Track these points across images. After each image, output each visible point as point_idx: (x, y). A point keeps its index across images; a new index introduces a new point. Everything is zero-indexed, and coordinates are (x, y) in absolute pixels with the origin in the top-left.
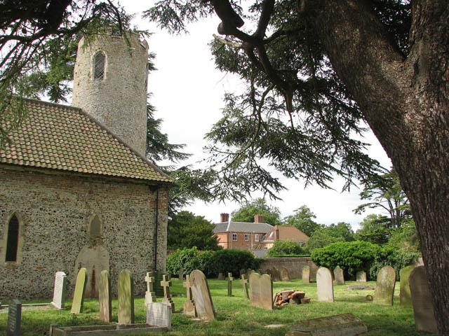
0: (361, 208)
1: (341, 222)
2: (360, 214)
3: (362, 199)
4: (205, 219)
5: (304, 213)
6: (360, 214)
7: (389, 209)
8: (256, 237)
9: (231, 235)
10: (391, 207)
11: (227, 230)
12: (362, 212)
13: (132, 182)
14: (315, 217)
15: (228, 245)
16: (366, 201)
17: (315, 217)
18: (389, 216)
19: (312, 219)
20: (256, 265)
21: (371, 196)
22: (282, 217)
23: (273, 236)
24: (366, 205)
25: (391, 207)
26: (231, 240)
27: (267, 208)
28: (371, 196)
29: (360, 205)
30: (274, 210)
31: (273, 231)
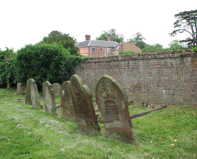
0: (174, 32)
1: (160, 44)
2: (174, 36)
3: (175, 27)
4: (69, 36)
5: (138, 37)
6: (174, 36)
7: (192, 33)
8: (108, 50)
9: (91, 48)
10: (193, 32)
11: (89, 45)
12: (175, 35)
13: (89, 62)
14: (145, 39)
15: (89, 55)
16: (177, 28)
17: (145, 39)
18: (192, 38)
19: (143, 40)
20: (173, 33)
21: (180, 25)
22: (125, 41)
23: (119, 49)
24: (178, 30)
25: (193, 32)
26: (91, 52)
27: (116, 35)
28: (180, 25)
29: (174, 30)
30: (121, 36)
31: (119, 45)
